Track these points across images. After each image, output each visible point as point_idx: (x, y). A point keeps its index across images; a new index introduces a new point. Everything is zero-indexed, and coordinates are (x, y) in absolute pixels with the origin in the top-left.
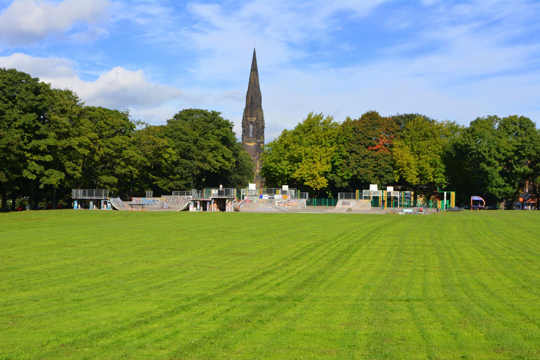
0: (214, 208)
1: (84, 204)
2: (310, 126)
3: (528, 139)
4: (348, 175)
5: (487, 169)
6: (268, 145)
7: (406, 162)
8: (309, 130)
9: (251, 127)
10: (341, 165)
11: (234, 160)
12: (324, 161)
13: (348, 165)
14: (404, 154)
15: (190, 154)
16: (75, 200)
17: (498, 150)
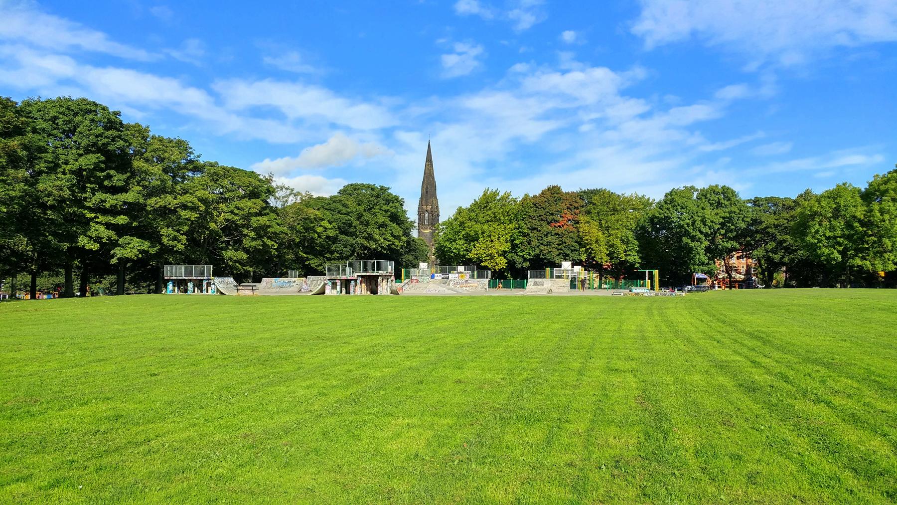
0: (360, 289)
1: (181, 284)
2: (487, 203)
3: (734, 209)
4: (529, 254)
5: (692, 244)
6: (443, 224)
7: (594, 239)
8: (486, 207)
9: (427, 215)
10: (521, 243)
11: (404, 239)
12: (503, 239)
13: (529, 243)
14: (591, 230)
15: (352, 230)
16: (168, 281)
17: (704, 222)
